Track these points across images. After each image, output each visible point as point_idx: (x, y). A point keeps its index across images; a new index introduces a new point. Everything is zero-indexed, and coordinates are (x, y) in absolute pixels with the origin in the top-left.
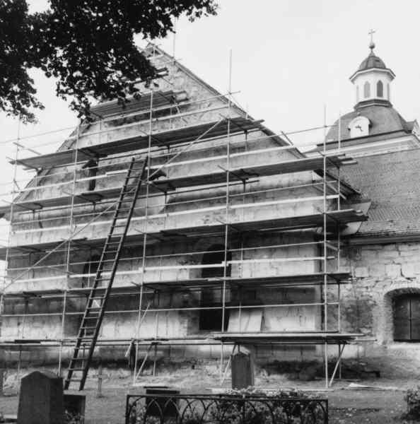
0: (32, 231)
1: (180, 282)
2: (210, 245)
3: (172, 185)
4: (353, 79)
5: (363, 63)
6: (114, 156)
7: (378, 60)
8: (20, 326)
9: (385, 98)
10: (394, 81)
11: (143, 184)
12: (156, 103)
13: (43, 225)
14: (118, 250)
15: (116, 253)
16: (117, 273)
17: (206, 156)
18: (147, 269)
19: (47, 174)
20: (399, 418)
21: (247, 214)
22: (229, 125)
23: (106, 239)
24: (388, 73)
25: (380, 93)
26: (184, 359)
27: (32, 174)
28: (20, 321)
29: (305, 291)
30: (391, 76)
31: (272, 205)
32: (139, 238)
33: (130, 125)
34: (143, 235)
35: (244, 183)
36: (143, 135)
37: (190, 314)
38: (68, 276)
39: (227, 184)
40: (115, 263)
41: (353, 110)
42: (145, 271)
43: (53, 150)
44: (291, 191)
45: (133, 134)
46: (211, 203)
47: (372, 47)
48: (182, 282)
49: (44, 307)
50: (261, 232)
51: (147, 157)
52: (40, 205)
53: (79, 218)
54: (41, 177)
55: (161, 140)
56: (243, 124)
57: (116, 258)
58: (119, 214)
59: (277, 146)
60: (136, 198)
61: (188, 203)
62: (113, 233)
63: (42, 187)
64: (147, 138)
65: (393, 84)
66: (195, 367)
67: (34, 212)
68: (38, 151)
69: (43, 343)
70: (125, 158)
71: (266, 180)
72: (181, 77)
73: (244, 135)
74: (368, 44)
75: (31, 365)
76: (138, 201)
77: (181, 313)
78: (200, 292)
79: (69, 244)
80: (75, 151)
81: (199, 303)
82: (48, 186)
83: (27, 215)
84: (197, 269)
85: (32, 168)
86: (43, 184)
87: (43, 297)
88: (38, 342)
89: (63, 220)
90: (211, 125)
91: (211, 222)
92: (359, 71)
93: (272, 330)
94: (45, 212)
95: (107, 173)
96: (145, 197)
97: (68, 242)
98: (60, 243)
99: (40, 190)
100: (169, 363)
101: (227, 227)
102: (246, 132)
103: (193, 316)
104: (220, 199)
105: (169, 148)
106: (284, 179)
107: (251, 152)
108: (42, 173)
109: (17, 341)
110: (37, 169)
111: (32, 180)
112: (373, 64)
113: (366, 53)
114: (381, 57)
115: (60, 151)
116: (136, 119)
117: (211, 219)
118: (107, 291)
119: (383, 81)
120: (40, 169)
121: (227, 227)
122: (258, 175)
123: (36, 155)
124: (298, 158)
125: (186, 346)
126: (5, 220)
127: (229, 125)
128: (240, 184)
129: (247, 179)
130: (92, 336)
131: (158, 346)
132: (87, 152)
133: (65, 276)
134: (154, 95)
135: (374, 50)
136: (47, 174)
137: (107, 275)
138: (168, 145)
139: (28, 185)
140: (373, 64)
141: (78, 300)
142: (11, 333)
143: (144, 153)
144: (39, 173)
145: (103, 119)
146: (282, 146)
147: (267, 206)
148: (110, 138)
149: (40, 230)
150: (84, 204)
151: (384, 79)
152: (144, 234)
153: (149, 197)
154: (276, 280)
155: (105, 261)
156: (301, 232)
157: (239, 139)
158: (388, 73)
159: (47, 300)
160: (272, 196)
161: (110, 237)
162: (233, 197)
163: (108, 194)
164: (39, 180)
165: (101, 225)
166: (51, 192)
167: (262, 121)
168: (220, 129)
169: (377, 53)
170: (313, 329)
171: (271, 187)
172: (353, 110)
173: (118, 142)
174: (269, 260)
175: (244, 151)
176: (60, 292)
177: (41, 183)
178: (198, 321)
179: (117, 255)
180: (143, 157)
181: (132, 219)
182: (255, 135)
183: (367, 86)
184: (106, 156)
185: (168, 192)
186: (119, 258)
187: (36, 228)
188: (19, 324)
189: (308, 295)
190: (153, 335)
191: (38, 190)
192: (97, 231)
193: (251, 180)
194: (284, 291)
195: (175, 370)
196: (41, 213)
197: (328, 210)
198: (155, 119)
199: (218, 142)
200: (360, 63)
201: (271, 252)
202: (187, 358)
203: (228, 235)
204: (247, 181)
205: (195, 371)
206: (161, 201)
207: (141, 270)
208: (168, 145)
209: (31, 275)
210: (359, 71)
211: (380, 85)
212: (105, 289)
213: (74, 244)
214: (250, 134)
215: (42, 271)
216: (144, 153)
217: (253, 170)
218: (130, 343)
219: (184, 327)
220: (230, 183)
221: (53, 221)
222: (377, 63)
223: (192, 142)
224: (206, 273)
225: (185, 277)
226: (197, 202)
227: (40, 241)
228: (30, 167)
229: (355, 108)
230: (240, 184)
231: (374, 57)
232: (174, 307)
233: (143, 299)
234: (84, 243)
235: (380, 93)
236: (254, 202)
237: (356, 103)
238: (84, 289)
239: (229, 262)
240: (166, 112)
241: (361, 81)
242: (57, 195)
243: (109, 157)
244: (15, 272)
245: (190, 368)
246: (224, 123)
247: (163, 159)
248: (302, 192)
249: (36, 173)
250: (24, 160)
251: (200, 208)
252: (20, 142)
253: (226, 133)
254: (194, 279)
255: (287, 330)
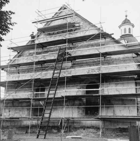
0: (15, 75)
1: (78, 96)
2: (89, 82)
3: (75, 58)
4: (120, 27)
5: (123, 21)
6: (49, 47)
7: (129, 21)
8: (10, 112)
9: (131, 34)
10: (134, 28)
11: (65, 57)
12: (69, 27)
13: (20, 73)
14: (57, 82)
15: (56, 84)
16: (57, 92)
17: (88, 47)
18: (67, 90)
19: (21, 53)
20: (95, 127)
21: (106, 69)
22: (101, 35)
23: (51, 78)
24: (132, 25)
25: (130, 32)
26: (80, 126)
27: (16, 53)
28: (10, 110)
29: (131, 100)
30: (133, 26)
31: (116, 66)
32: (63, 78)
33: (55, 35)
34: (65, 77)
35: (105, 58)
36: (64, 38)
37: (82, 108)
38: (33, 93)
39: (66, 62)
40: (56, 87)
41: (120, 38)
42: (66, 91)
43: (24, 44)
44: (124, 60)
45: (60, 38)
46: (90, 65)
47: (126, 16)
48: (79, 96)
49: (20, 105)
50: (113, 77)
51: (66, 47)
52: (19, 65)
53: (37, 70)
54: (19, 54)
55: (72, 41)
56: (105, 35)
57: (56, 86)
58: (55, 69)
59: (117, 44)
60: (63, 63)
61: (81, 65)
62: (54, 76)
63: (19, 58)
64: (65, 40)
65: (133, 29)
66: (85, 129)
67: (16, 68)
68: (18, 45)
69: (20, 119)
70: (58, 47)
71: (114, 57)
72: (76, 18)
73: (104, 40)
74: (125, 15)
75: (14, 127)
76: (63, 64)
77: (78, 108)
78: (85, 100)
79: (33, 80)
80: (35, 44)
81: (85, 104)
82: (21, 58)
83: (13, 69)
84: (84, 91)
85: (16, 51)
86: (20, 57)
87: (20, 101)
88: (18, 118)
89: (29, 71)
90: (93, 35)
91: (90, 73)
92: (122, 24)
93: (117, 115)
94: (21, 68)
95: (49, 53)
96: (66, 63)
97: (33, 79)
98: (29, 80)
99: (18, 59)
100: (74, 127)
101: (101, 74)
102: (105, 39)
103: (83, 109)
104: (97, 63)
105: (73, 44)
106: (121, 56)
107: (107, 46)
108: (20, 53)
109: (10, 118)
110: (17, 51)
111: (16, 55)
112: (126, 22)
113: (124, 18)
114: (130, 20)
115: (27, 45)
116: (58, 33)
117: (90, 72)
118: (53, 98)
119: (130, 28)
120: (19, 51)
121: (101, 74)
122: (111, 55)
123: (17, 46)
124: (128, 48)
125: (81, 121)
126: (4, 71)
127: (101, 35)
128: (103, 58)
129: (106, 56)
130: (42, 117)
131: (69, 121)
132: (40, 45)
133: (32, 93)
134: (68, 23)
135: (127, 17)
136: (21, 53)
137: (46, 92)
138: (72, 43)
139: (14, 58)
140: (126, 22)
141: (34, 102)
142: (6, 114)
143: (65, 46)
144: (18, 53)
145: (45, 33)
146: (120, 43)
147: (114, 67)
148: (48, 40)
149: (18, 75)
150: (37, 65)
151: (131, 27)
152: (65, 77)
153: (67, 63)
154: (128, 95)
155: (51, 87)
156: (129, 77)
157: (101, 41)
158: (132, 25)
159: (21, 102)
160: (116, 63)
161: (53, 77)
162: (36, 70)
163: (53, 61)
164: (18, 56)
165: (45, 73)
166: (23, 60)
167: (113, 34)
168: (97, 37)
169: (128, 18)
170: (136, 115)
171: (116, 59)
172: (120, 38)
173: (53, 41)
174: (116, 88)
175: (104, 45)
176: (29, 99)
177: (20, 56)
178: (85, 111)
179: (56, 85)
180: (64, 47)
181: (61, 71)
182: (108, 40)
183: (125, 30)
184: (46, 47)
185: (73, 61)
186: (57, 85)
187: (17, 74)
188: (9, 111)
189: (133, 102)
190: (67, 116)
191: (18, 59)
192: (43, 76)
193: (107, 57)
194: (123, 100)
195: (76, 130)
196: (19, 68)
197: (137, 69)
198: (69, 33)
199: (96, 42)
200: (122, 21)
201: (116, 84)
202: (81, 126)
203: (101, 77)
204: (106, 57)
205: (85, 131)
206: (70, 64)
207: (64, 91)
208: (72, 43)
209: (15, 92)
210: (122, 24)
211: (130, 29)
212: (46, 98)
213: (35, 80)
214: (106, 39)
215: (19, 91)
216: (65, 46)
217: (110, 52)
218: (60, 119)
219: (80, 114)
220: (67, 62)
221: (24, 71)
222: (128, 22)
223: (85, 42)
224: (87, 92)
225: (80, 94)
226: (39, 70)
227: (18, 79)
228: (15, 51)
229: (120, 37)
230: (103, 58)
231: (127, 19)
232: (75, 106)
233: (86, 107)
234: (39, 80)
235: (130, 32)
236: (108, 65)
237: (121, 35)
238: (36, 98)
239: (102, 88)
240: (71, 30)
241: (123, 28)
242: (25, 61)
243: (47, 47)
244: (8, 91)
245: (83, 129)
246: (99, 34)
247: (71, 48)
248: (129, 62)
249: (17, 53)
250: (14, 48)
251: (85, 67)
252: (12, 41)
253: (100, 38)
254: (83, 94)
255: (124, 115)
